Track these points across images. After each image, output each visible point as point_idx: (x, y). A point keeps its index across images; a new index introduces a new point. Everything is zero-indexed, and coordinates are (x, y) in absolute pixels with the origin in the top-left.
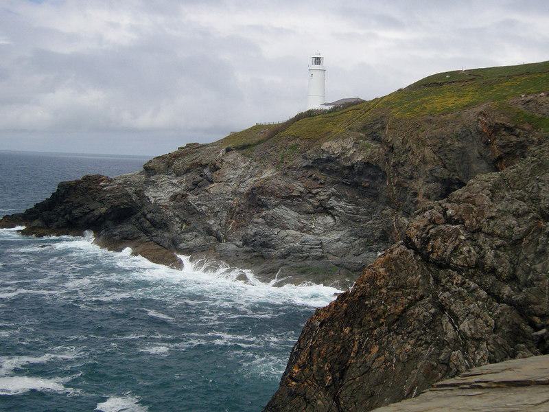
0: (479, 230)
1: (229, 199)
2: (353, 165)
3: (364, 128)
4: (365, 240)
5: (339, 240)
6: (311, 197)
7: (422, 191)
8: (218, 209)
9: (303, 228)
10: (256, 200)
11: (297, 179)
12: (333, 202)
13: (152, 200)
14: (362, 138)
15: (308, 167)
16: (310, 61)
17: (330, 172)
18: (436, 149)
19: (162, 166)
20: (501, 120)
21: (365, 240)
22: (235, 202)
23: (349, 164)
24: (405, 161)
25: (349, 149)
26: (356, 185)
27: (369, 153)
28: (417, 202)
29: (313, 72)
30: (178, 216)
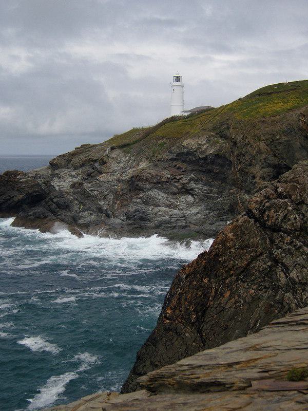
2: (206, 157)
3: (214, 129)
4: (218, 212)
5: (198, 213)
6: (176, 182)
7: (259, 174)
8: (106, 193)
10: (135, 185)
11: (165, 169)
12: (193, 185)
13: (57, 188)
14: (212, 136)
18: (269, 142)
19: (63, 162)
21: (218, 212)
22: (119, 187)
23: (204, 156)
25: (203, 145)
26: (209, 172)
28: (255, 183)
30: (77, 199)
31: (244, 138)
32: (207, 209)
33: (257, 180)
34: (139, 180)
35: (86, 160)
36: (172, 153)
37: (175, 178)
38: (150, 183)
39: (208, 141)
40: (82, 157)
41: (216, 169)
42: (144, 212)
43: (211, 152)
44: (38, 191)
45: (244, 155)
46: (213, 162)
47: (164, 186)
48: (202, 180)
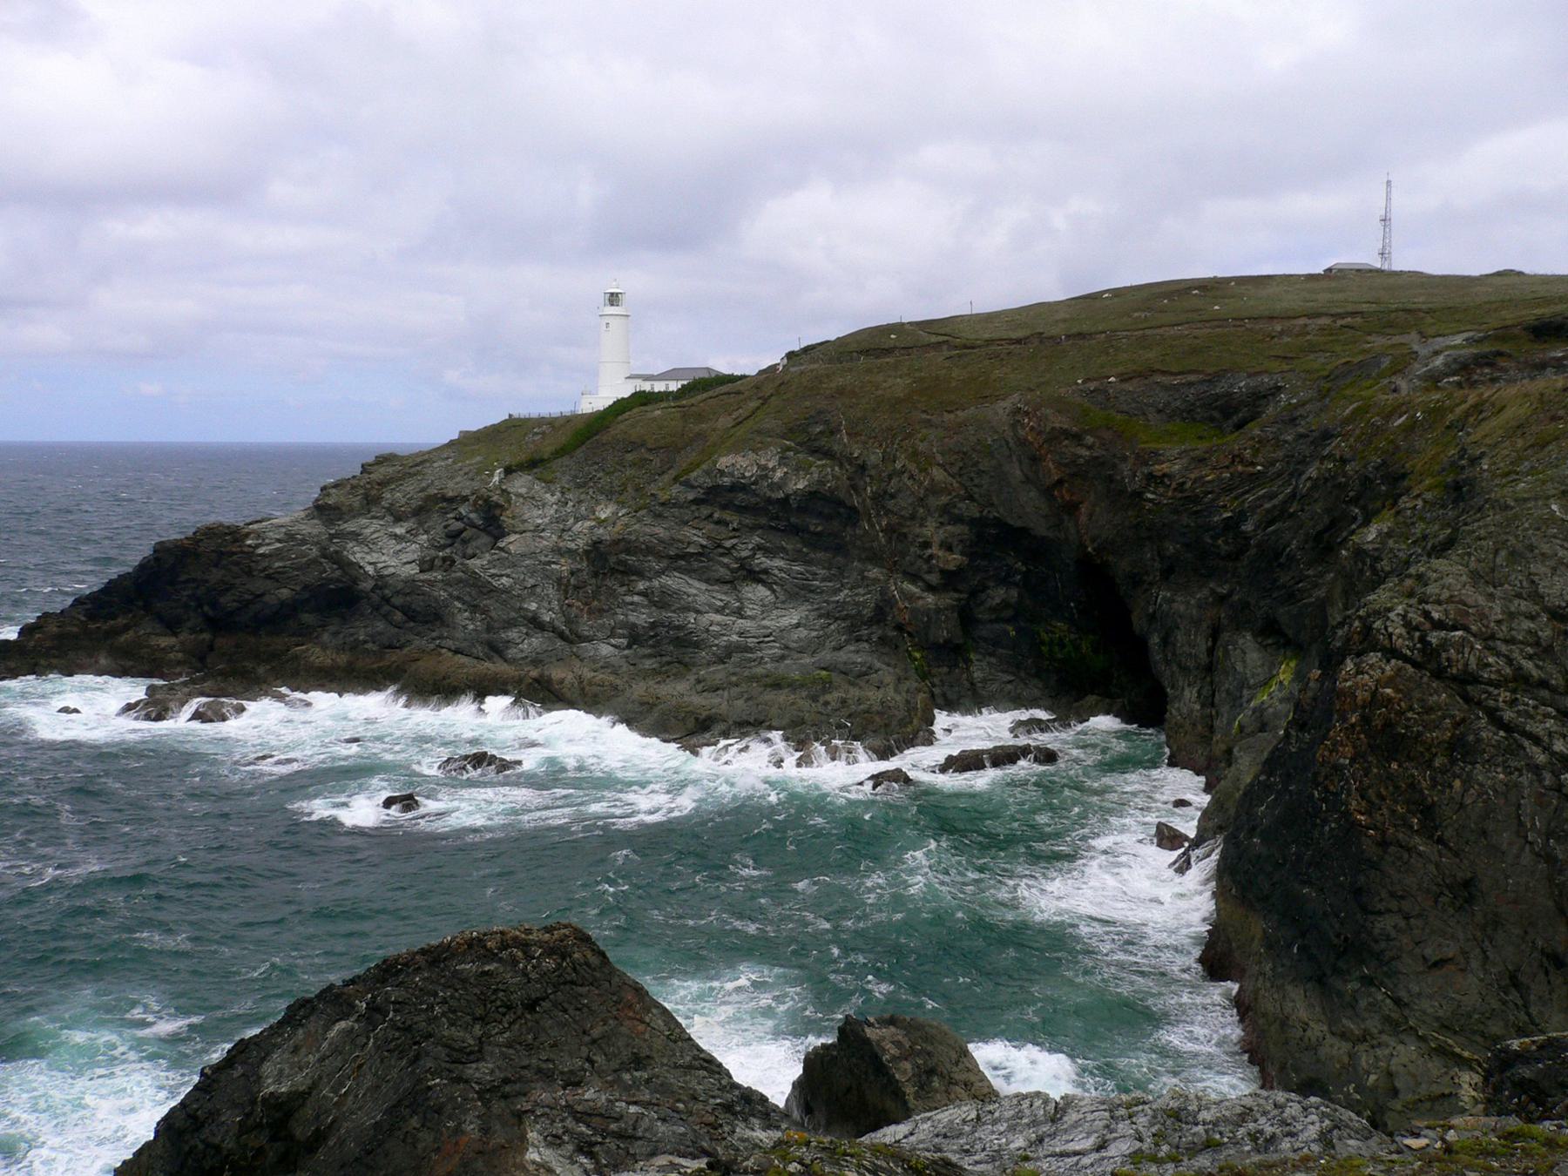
0: (1493, 637)
1: (549, 563)
2: (788, 496)
3: (790, 432)
4: (848, 623)
5: (798, 625)
6: (722, 555)
7: (936, 540)
8: (531, 582)
9: (723, 608)
10: (608, 563)
11: (686, 523)
12: (762, 561)
13: (370, 569)
14: (789, 449)
15: (696, 502)
16: (601, 299)
17: (742, 509)
18: (955, 470)
19: (356, 501)
20: (1060, 422)
21: (848, 623)
22: (563, 567)
23: (781, 495)
24: (899, 491)
25: (774, 470)
26: (795, 530)
27: (816, 476)
28: (931, 557)
29: (607, 320)
30: (458, 598)
31: (888, 458)
32: (820, 616)
33: (934, 550)
34: (628, 551)
35: (463, 492)
36: (693, 487)
37: (719, 546)
38: (659, 556)
39: (783, 461)
40: (411, 487)
41: (816, 525)
42: (679, 628)
43: (800, 486)
44: (338, 580)
45: (893, 496)
46: (802, 510)
47: (696, 565)
48: (784, 549)
